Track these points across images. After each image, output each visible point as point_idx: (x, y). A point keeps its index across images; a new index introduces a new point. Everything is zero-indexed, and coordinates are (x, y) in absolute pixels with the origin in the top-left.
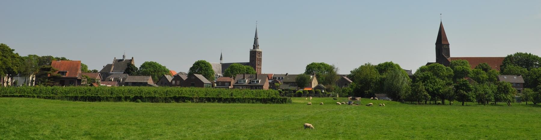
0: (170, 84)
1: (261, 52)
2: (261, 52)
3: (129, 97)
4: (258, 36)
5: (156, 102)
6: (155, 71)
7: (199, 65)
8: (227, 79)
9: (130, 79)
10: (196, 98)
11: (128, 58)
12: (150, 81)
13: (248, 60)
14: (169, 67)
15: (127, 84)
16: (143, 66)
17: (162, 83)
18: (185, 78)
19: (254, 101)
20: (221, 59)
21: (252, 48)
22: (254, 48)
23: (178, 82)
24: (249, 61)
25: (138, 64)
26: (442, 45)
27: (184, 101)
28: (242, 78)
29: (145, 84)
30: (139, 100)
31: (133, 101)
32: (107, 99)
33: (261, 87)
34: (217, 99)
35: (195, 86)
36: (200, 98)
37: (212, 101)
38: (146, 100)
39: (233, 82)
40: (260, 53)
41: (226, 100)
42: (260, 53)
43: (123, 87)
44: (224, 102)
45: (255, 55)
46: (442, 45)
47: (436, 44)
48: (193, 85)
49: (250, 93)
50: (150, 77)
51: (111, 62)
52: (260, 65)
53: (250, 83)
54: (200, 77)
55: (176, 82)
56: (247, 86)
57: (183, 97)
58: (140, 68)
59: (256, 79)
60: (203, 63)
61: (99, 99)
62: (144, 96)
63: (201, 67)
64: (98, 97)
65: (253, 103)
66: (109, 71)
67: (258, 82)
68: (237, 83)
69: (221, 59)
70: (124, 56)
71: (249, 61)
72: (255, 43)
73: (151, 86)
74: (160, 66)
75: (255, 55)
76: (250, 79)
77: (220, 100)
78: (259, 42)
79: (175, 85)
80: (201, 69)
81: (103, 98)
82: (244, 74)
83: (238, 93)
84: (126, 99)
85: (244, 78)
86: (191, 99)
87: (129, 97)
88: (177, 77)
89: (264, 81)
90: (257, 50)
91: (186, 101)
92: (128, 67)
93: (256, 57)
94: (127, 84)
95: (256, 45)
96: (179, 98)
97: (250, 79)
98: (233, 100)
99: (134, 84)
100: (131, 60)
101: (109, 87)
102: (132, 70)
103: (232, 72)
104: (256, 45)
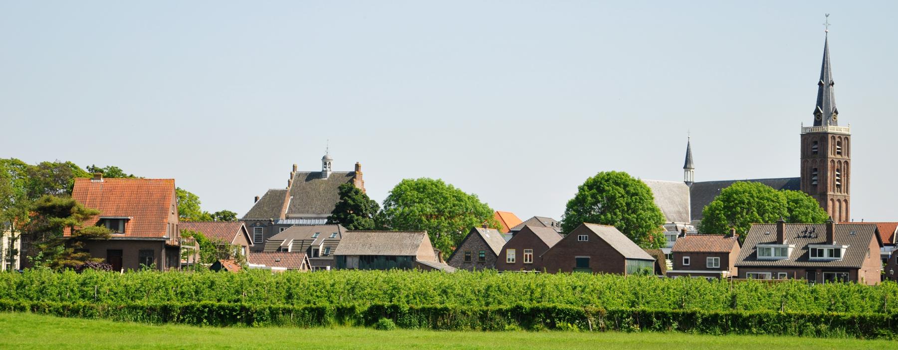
0: (498, 263)
1: (847, 138)
3: (353, 309)
4: (835, 74)
5: (449, 328)
6: (441, 212)
7: (601, 191)
8: (715, 243)
9: (352, 243)
10: (597, 314)
11: (341, 166)
12: (423, 249)
13: (794, 171)
14: (489, 197)
15: (341, 262)
16: (397, 196)
17: (468, 258)
18: (551, 238)
19: (823, 327)
20: (687, 165)
21: (810, 122)
22: (818, 122)
23: (528, 254)
24: (799, 176)
25: (377, 189)
27: (552, 326)
28: (773, 237)
29: (408, 263)
30: (388, 322)
31: (368, 324)
32: (274, 317)
33: (851, 273)
34: (675, 316)
35: (596, 271)
36: (611, 316)
37: (657, 324)
38: (415, 320)
39: (736, 255)
40: (843, 141)
41: (711, 324)
42: (843, 141)
43: (329, 276)
44: (702, 332)
45: (821, 152)
48: (583, 265)
49: (803, 298)
50: (425, 238)
51: (281, 184)
52: (843, 185)
53: (804, 258)
54: (611, 235)
55: (519, 255)
56: (791, 271)
57: (548, 312)
58: (387, 203)
59: (829, 241)
60: (619, 181)
61: (248, 317)
62: (406, 308)
63: (608, 198)
64: (243, 308)
65: (818, 333)
66: (278, 217)
67: (837, 252)
68: (753, 257)
69: (687, 165)
70: (325, 161)
71: (799, 176)
72: (820, 102)
73: (428, 268)
74: (459, 197)
75: (821, 152)
76: (803, 242)
77: (687, 322)
78: (839, 97)
79: (517, 266)
80: (611, 204)
81: (260, 313)
82: (780, 224)
83: (757, 297)
84: (342, 314)
85: (780, 240)
86: (578, 318)
87: (353, 309)
88: (523, 237)
89: (861, 251)
90: (831, 129)
91: (559, 324)
92: (348, 207)
93: (825, 157)
94: (341, 262)
95: (824, 110)
96: (535, 312)
97: (803, 242)
98: (739, 324)
99: (368, 262)
100: (352, 175)
101: (278, 274)
102: (357, 209)
103: (732, 217)
104: (824, 110)
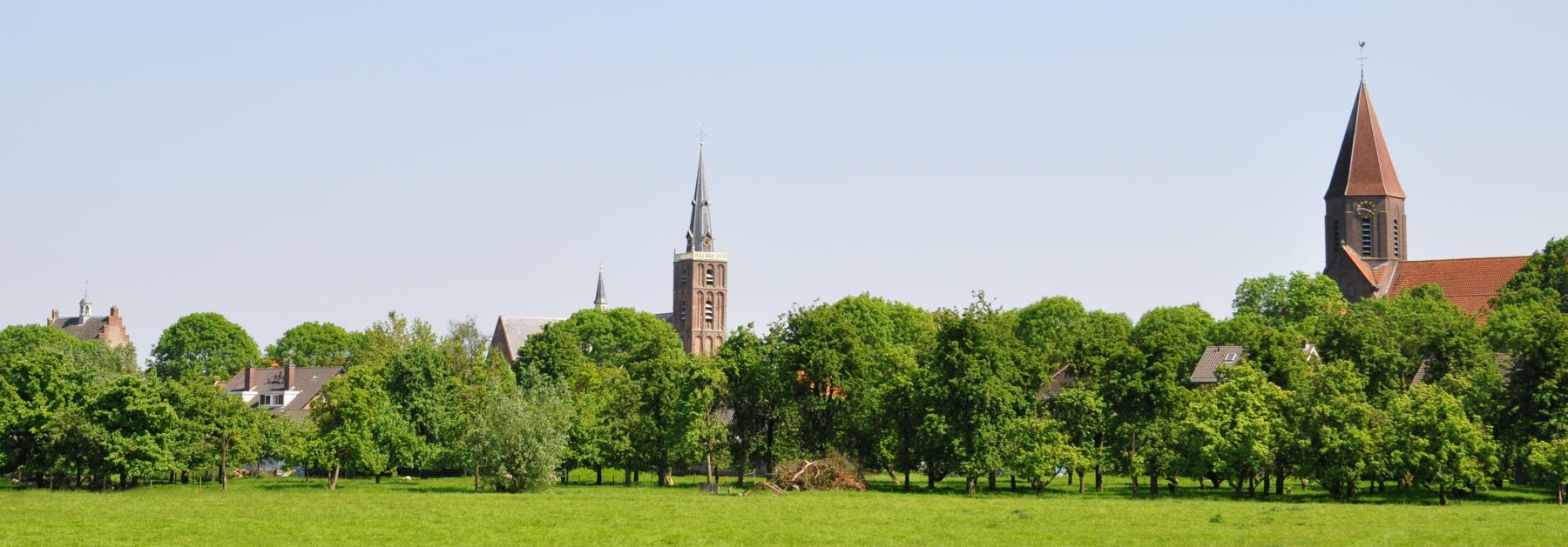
2: (722, 265)
4: (710, 194)
24: (1409, 258)
26: (1357, 203)
42: (716, 270)
46: (1357, 203)
47: (1327, 198)
78: (715, 219)
95: (698, 236)
104: (698, 236)
